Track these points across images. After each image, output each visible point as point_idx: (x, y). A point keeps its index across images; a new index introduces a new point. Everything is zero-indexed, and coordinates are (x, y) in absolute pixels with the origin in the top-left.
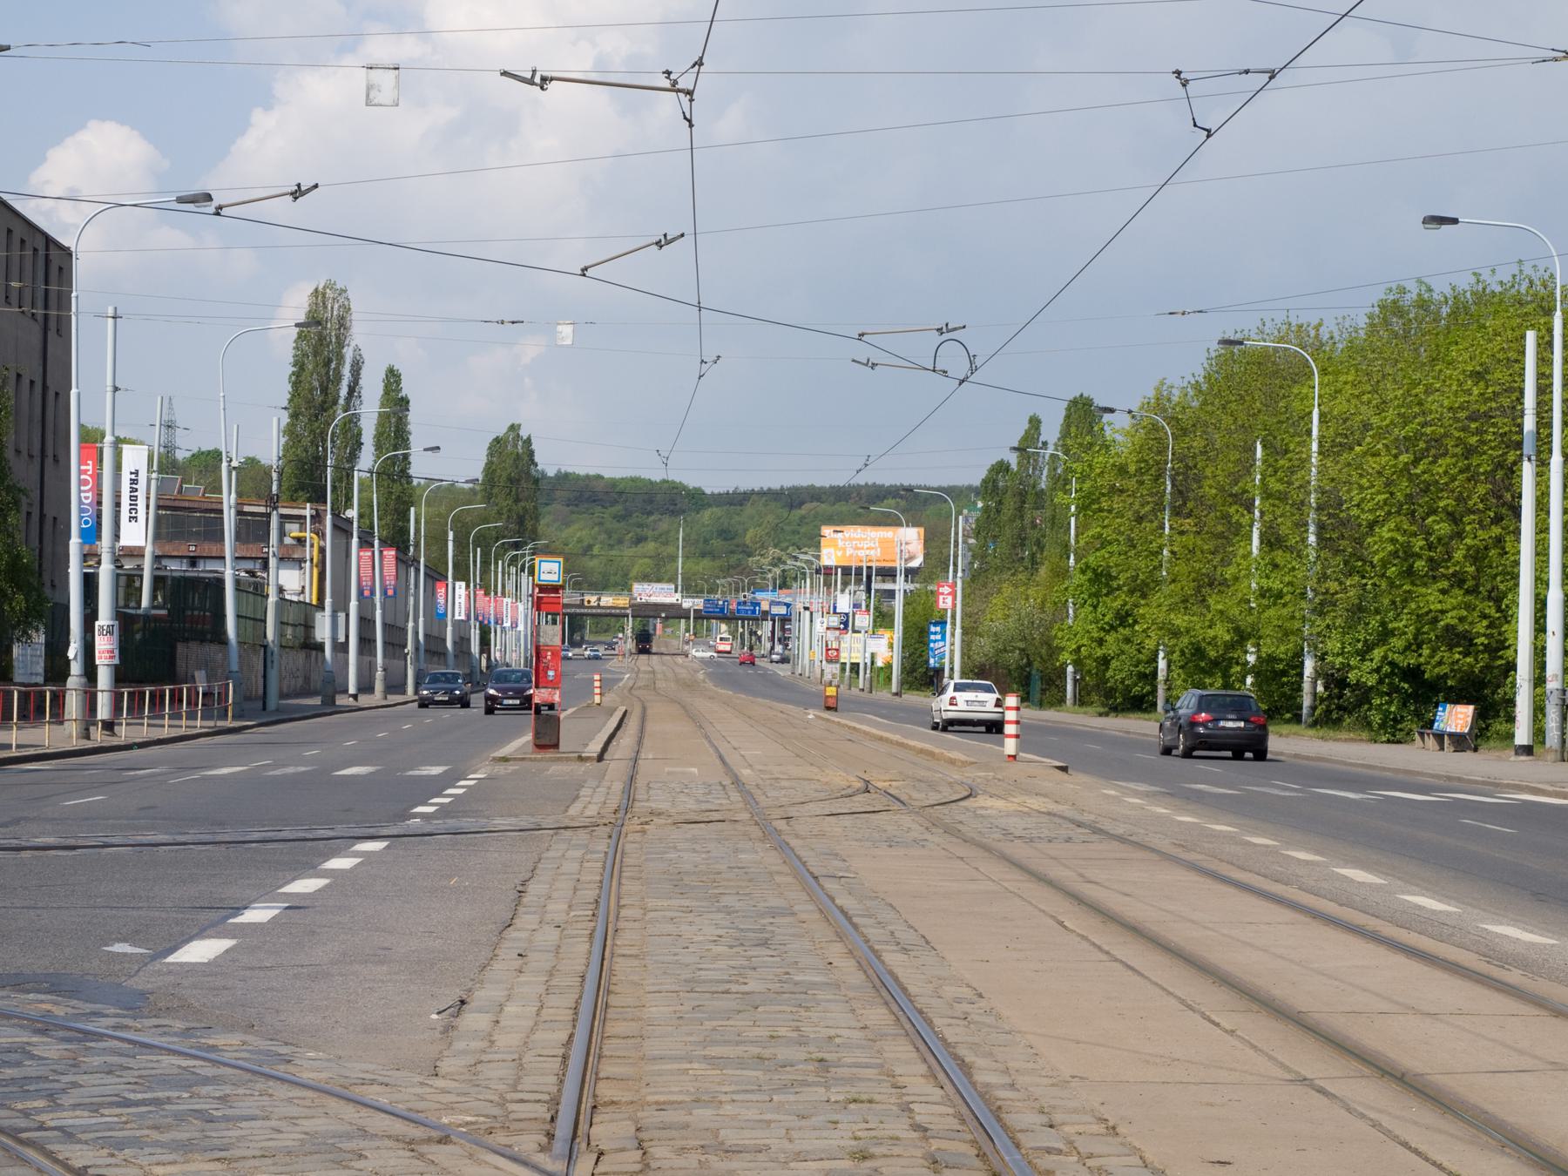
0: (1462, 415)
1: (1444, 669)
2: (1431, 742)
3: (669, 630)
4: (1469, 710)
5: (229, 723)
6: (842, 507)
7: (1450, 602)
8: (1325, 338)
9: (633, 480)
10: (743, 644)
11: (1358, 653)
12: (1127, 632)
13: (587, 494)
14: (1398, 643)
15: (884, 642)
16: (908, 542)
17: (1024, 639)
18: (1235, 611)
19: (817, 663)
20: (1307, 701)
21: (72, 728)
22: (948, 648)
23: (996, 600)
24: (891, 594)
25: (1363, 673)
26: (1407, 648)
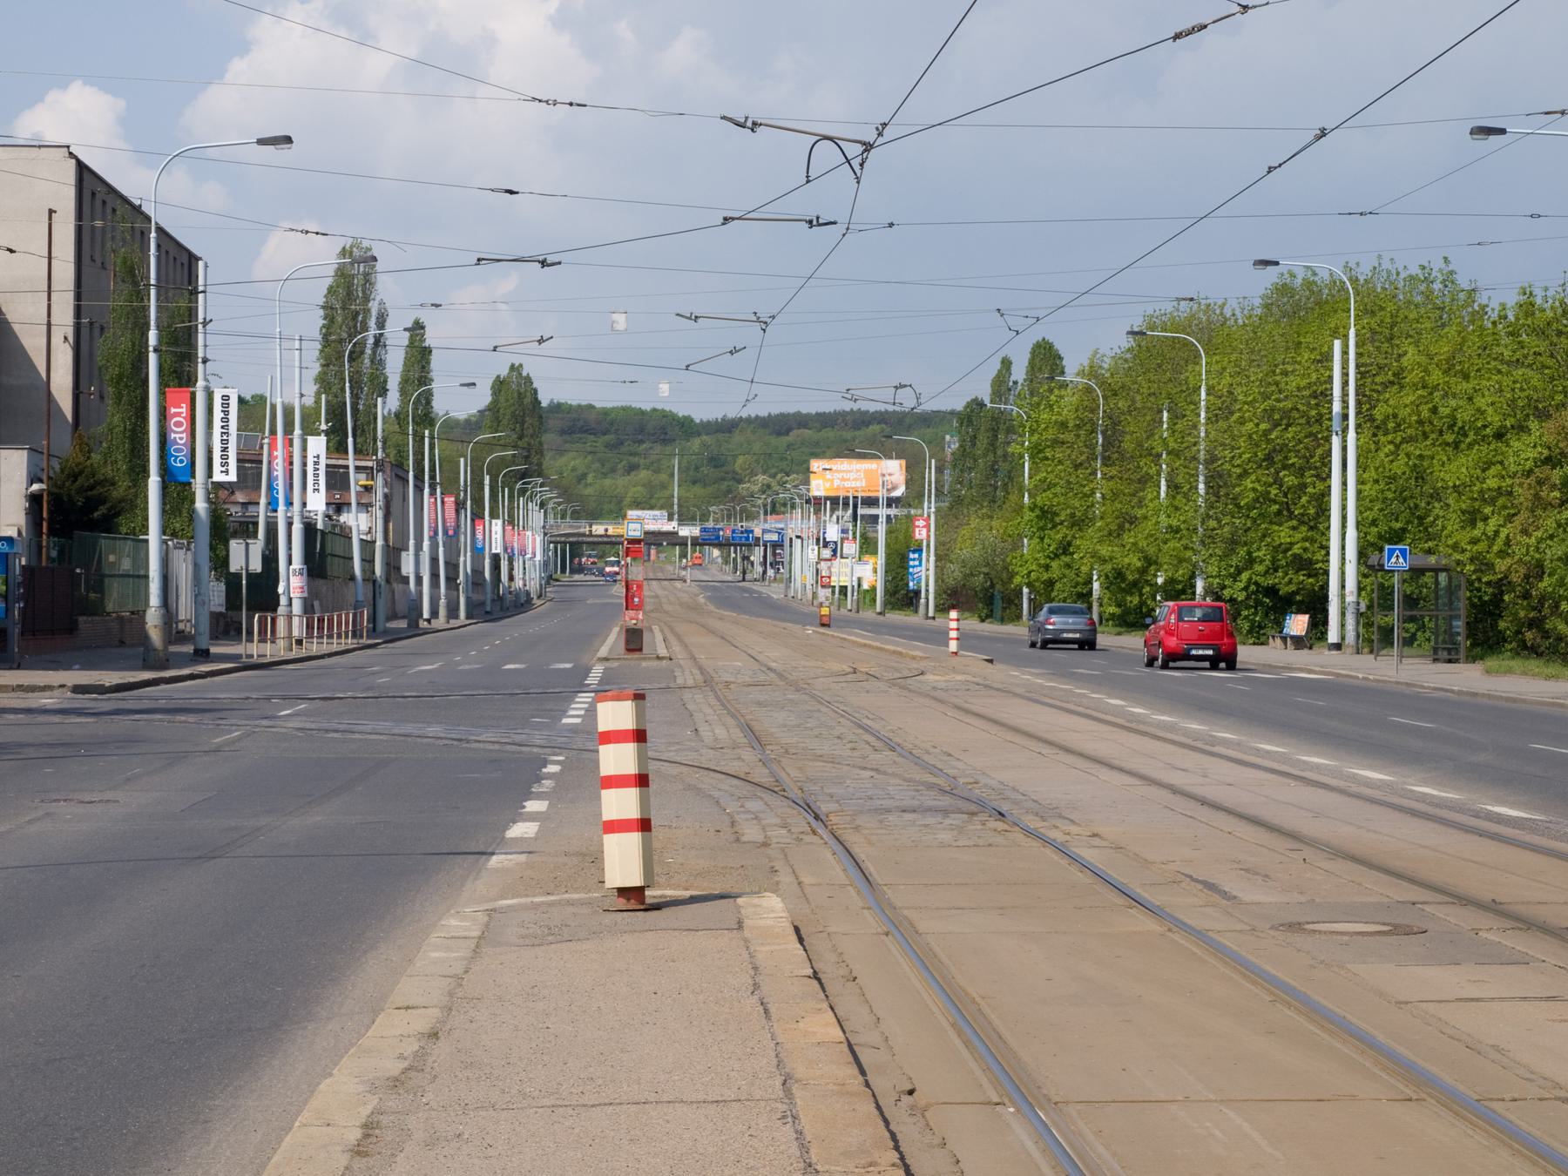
0: (1307, 393)
1: (1293, 588)
2: (1278, 641)
3: (662, 556)
4: (1306, 618)
5: (365, 641)
6: (828, 434)
8: (1228, 313)
9: (624, 409)
10: (736, 570)
11: (1231, 575)
12: (1067, 559)
13: (583, 424)
14: (1259, 568)
15: (869, 567)
16: (892, 472)
18: (1143, 544)
19: (809, 587)
21: (281, 643)
22: (924, 573)
23: (965, 531)
24: (875, 518)
26: (1267, 572)
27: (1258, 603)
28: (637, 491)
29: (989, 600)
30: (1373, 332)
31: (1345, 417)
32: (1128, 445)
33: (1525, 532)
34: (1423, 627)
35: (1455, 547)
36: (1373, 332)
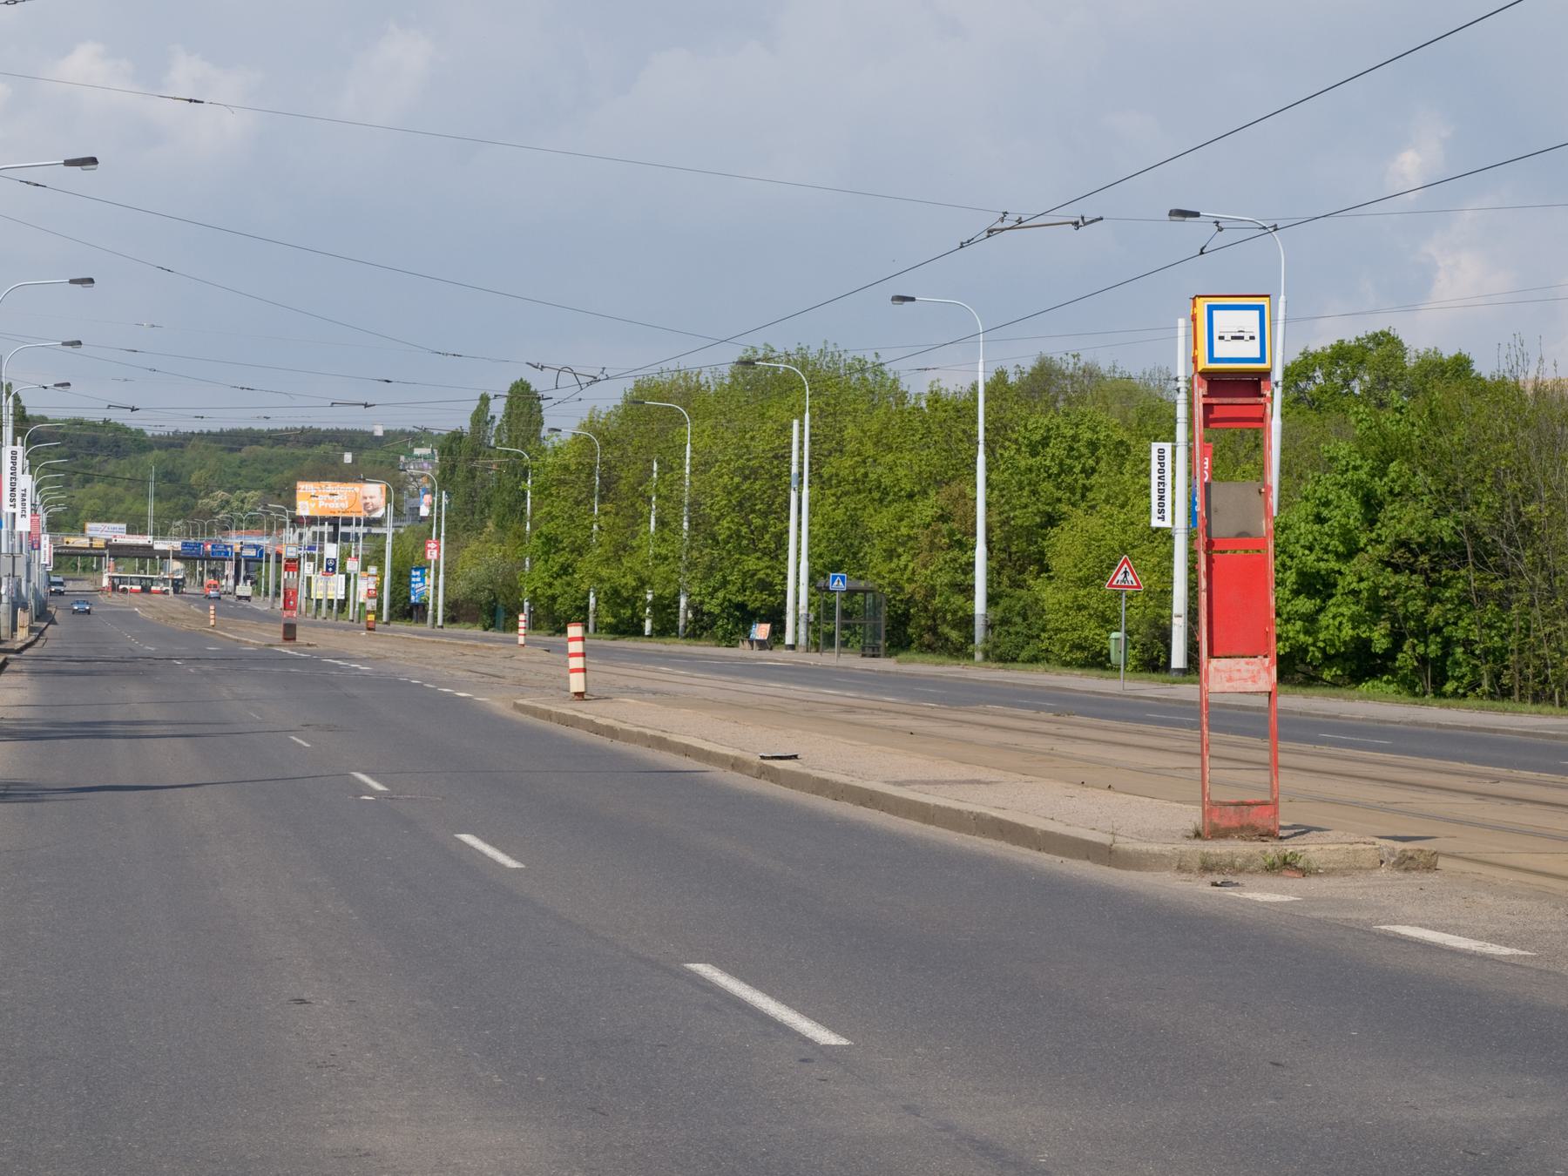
1: (758, 604)
2: (747, 644)
4: (768, 626)
7: (762, 564)
8: (703, 381)
17: (491, 582)
18: (638, 567)
20: (681, 623)
23: (466, 553)
25: (712, 606)
27: (730, 615)
28: (90, 504)
29: (493, 613)
30: (822, 410)
31: (801, 474)
32: (623, 487)
33: (925, 566)
34: (855, 633)
35: (878, 575)
36: (822, 410)
